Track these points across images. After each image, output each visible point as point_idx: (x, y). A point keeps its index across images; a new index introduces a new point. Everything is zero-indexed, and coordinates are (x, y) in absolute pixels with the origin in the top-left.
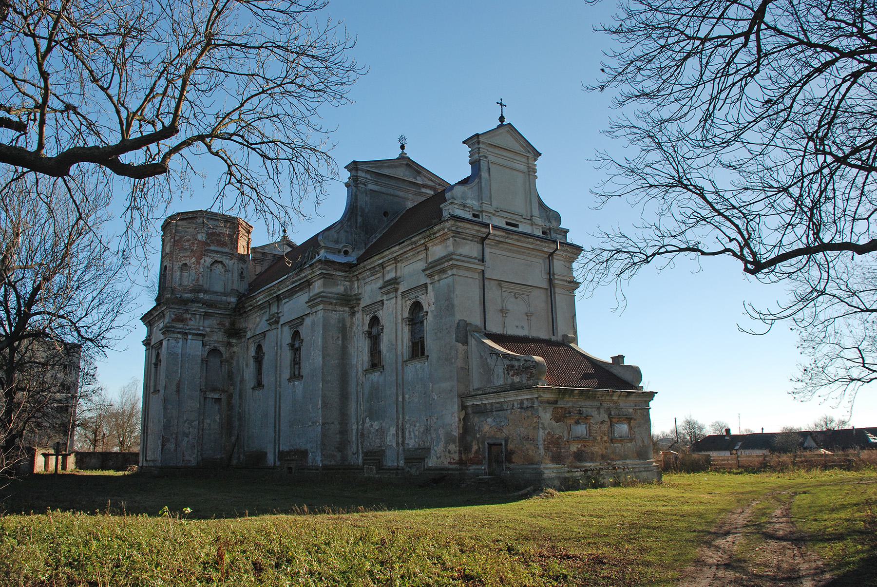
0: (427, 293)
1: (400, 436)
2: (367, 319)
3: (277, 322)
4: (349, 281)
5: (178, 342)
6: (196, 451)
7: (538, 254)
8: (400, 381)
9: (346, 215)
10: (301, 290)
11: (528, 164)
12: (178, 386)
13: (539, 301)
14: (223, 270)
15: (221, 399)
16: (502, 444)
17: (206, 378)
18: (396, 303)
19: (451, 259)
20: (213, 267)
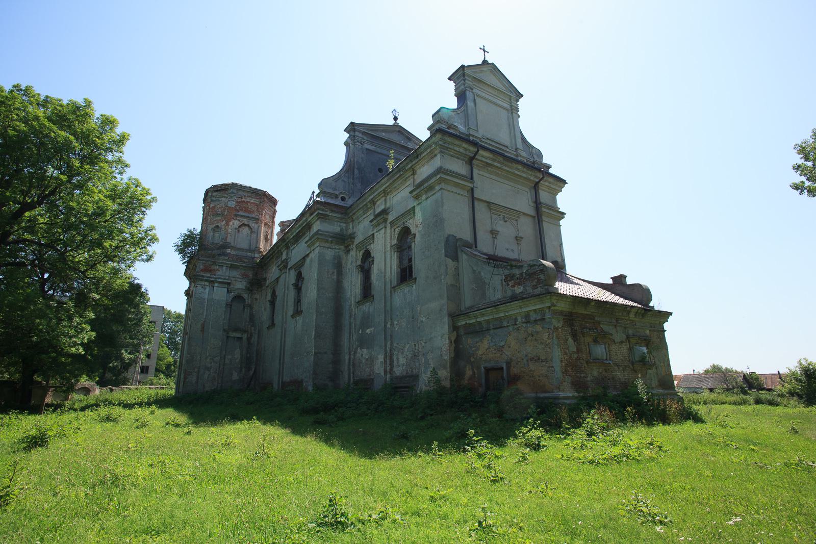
0: (414, 216)
1: (388, 363)
2: (360, 254)
3: (286, 267)
4: (345, 223)
5: (205, 289)
6: (216, 383)
7: (524, 181)
8: (388, 308)
11: (511, 103)
12: (203, 327)
13: (526, 227)
14: (249, 232)
16: (502, 369)
17: (229, 320)
18: (385, 233)
20: (241, 229)
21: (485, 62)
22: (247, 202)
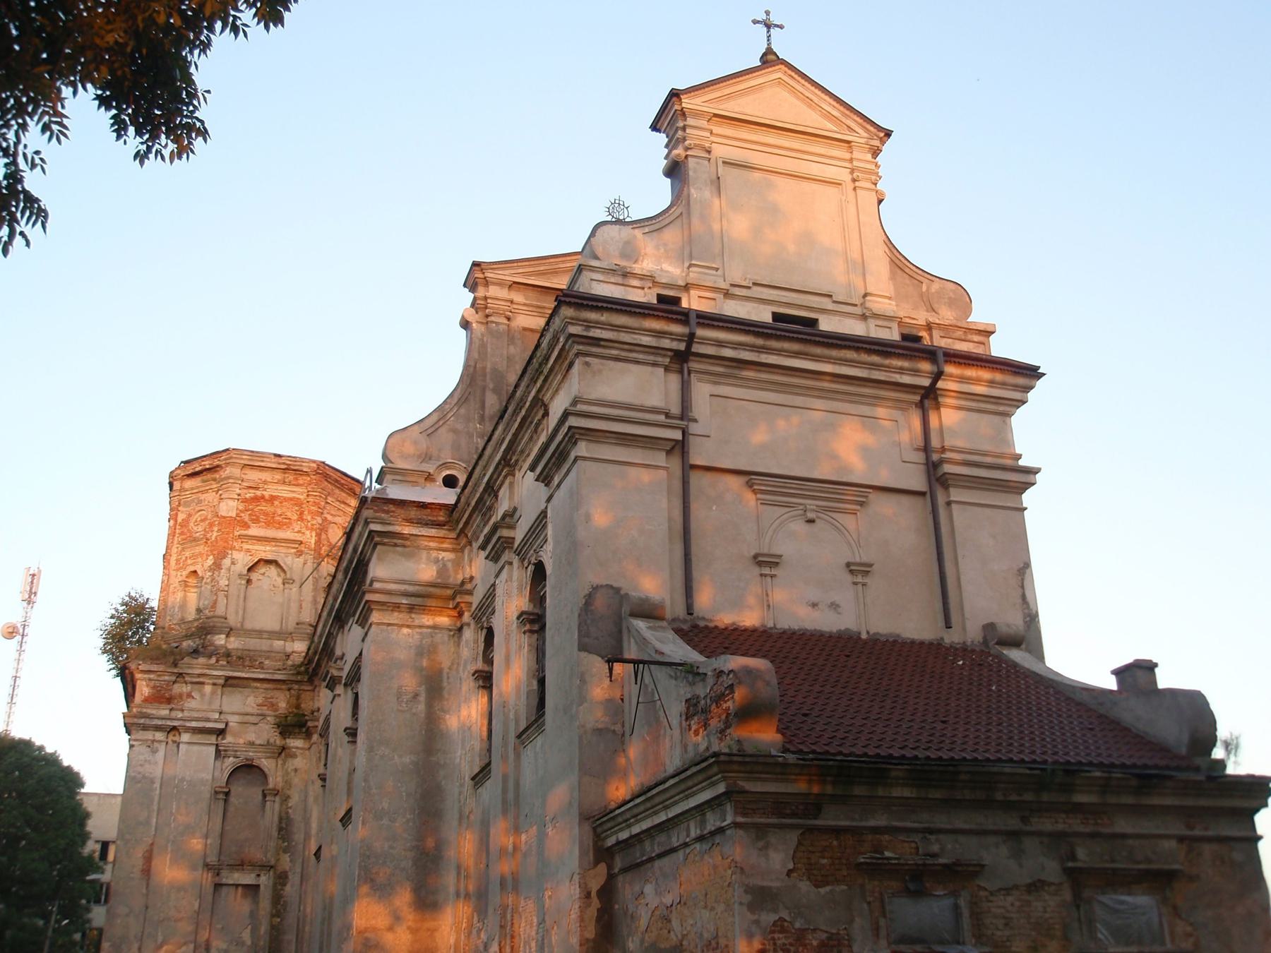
5: (155, 752)
14: (280, 581)
15: (258, 886)
17: (222, 835)
20: (254, 576)
21: (769, 59)
22: (273, 499)
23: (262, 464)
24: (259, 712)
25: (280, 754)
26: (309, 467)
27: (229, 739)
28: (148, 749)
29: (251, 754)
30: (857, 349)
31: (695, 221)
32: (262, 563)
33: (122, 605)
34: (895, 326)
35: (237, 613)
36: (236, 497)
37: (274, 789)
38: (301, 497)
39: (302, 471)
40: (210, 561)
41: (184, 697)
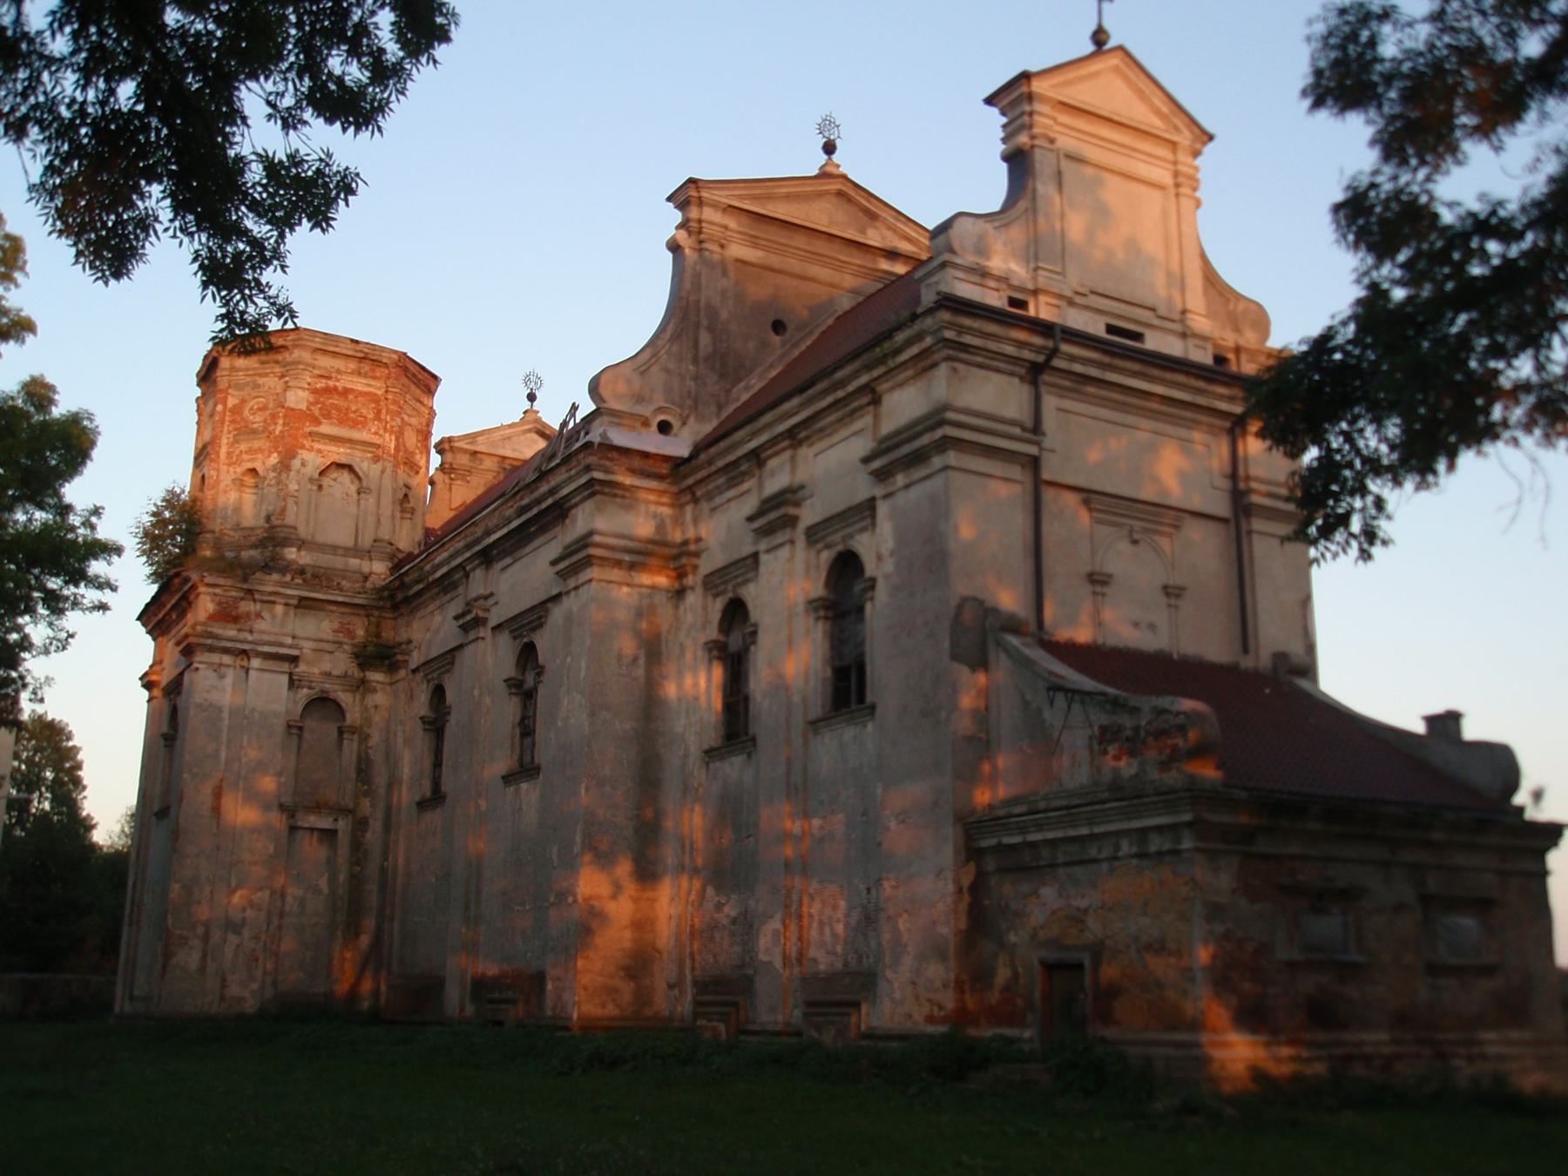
0: (874, 525)
2: (717, 607)
5: (222, 677)
9: (670, 319)
10: (543, 530)
14: (353, 488)
15: (334, 832)
18: (791, 559)
19: (943, 423)
20: (326, 481)
22: (346, 392)
23: (337, 350)
24: (336, 639)
25: (358, 687)
26: (390, 358)
27: (302, 668)
28: (215, 674)
29: (327, 686)
30: (1187, 374)
31: (1041, 221)
32: (333, 467)
33: (163, 501)
34: (1209, 347)
35: (308, 522)
36: (306, 386)
37: (351, 727)
38: (379, 392)
39: (380, 362)
40: (274, 459)
41: (253, 617)
